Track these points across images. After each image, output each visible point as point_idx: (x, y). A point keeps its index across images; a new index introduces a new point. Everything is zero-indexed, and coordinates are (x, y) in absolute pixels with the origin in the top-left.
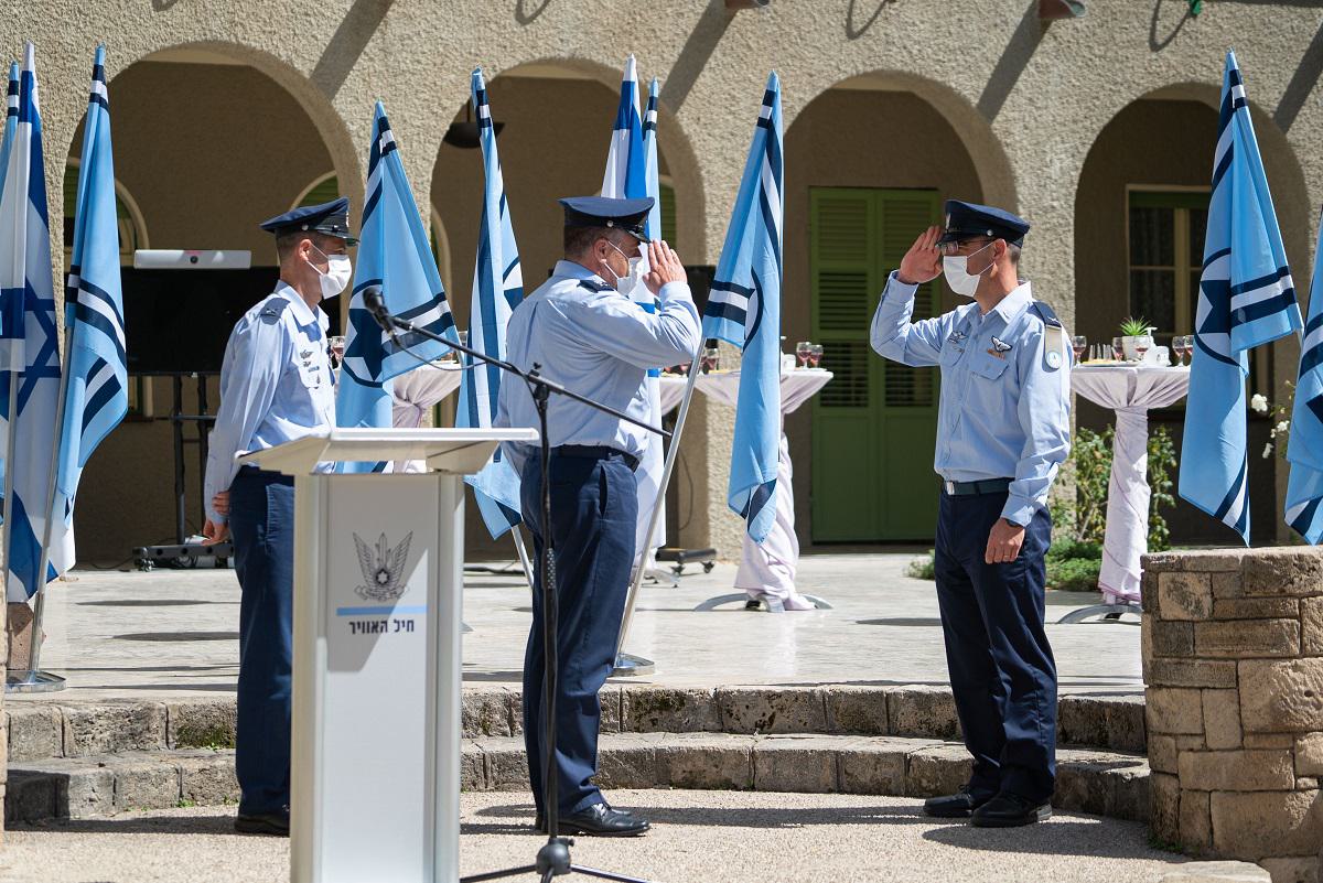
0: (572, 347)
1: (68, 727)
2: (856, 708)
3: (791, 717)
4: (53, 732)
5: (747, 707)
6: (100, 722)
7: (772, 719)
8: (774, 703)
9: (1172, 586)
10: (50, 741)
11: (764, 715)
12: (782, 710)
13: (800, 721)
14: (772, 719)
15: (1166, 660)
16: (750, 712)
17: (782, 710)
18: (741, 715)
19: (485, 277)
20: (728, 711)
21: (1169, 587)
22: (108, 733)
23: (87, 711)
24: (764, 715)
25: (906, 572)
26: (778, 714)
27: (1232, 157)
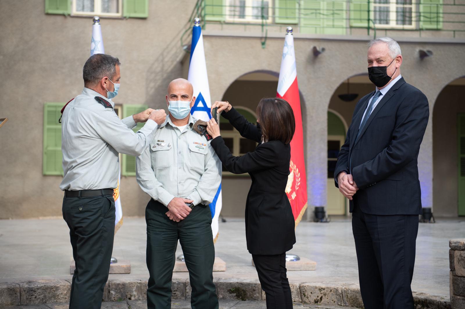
0: (94, 163)
1: (23, 293)
2: (355, 296)
3: (329, 298)
4: (15, 295)
5: (311, 293)
6: (39, 291)
7: (321, 298)
8: (322, 292)
9: (460, 258)
10: (14, 299)
11: (318, 297)
12: (325, 295)
13: (333, 300)
14: (321, 298)
15: (458, 297)
16: (312, 295)
17: (325, 295)
18: (309, 296)
19: (81, 128)
20: (304, 294)
21: (458, 259)
22: (43, 295)
23: (34, 286)
24: (318, 297)
25: (229, 288)
26: (323, 297)
27: (4, 120)
